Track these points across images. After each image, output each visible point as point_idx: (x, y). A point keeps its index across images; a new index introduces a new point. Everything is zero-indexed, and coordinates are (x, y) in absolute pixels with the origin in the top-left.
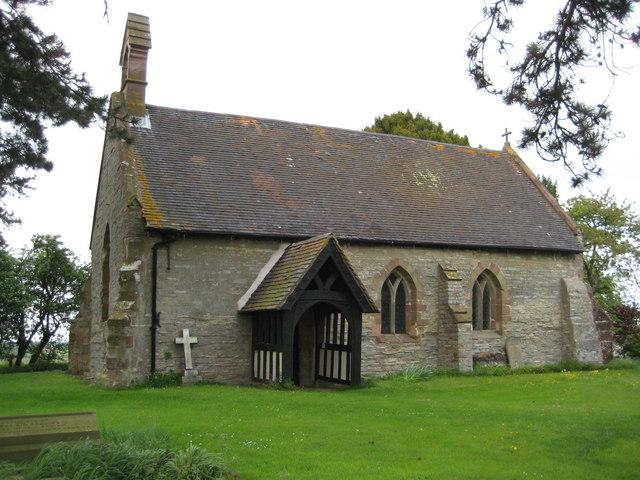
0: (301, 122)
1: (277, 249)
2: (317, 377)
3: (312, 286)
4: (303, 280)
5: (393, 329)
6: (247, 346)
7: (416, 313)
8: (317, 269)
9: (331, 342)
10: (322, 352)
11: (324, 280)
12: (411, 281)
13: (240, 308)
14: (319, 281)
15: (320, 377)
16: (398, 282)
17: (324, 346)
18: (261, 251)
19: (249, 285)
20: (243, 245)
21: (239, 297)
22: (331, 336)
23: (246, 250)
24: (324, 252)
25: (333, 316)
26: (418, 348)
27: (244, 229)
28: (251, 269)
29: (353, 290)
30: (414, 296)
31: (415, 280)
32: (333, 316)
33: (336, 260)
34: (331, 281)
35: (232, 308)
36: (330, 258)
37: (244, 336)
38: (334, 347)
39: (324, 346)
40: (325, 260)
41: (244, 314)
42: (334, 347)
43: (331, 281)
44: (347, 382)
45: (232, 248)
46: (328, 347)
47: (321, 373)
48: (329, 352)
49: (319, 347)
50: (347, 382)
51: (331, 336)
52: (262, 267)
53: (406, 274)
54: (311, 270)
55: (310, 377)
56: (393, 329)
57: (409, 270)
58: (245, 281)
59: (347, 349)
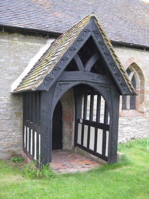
0: (84, 135)
1: (45, 43)
2: (76, 144)
3: (72, 67)
4: (63, 59)
5: (128, 106)
6: (20, 122)
7: (144, 96)
8: (78, 49)
9: (88, 118)
10: (80, 126)
11: (84, 63)
12: (141, 74)
13: (12, 91)
14: (79, 62)
15: (78, 145)
16: (132, 74)
17: (81, 121)
18: (32, 44)
19: (21, 71)
20: (16, 39)
21: (11, 81)
22: (88, 112)
23: (18, 42)
24: (85, 31)
25: (89, 97)
26: (144, 119)
27: (15, 23)
28: (23, 58)
29: (114, 73)
30: (142, 84)
31: (144, 73)
32: (89, 97)
33: (97, 41)
34: (91, 63)
35: (7, 90)
36: (91, 38)
37: (16, 113)
38: (90, 123)
39: (81, 121)
40: (86, 39)
41: (16, 95)
42: (90, 123)
43: (91, 63)
44: (102, 157)
45: (7, 41)
46: (85, 122)
47: (79, 142)
48: (86, 127)
49: (77, 122)
50: (102, 157)
51: (88, 112)
52: (33, 56)
53: (138, 68)
54: (71, 49)
55: (70, 144)
56: (128, 106)
57: (140, 65)
58: (17, 68)
59: (105, 127)
